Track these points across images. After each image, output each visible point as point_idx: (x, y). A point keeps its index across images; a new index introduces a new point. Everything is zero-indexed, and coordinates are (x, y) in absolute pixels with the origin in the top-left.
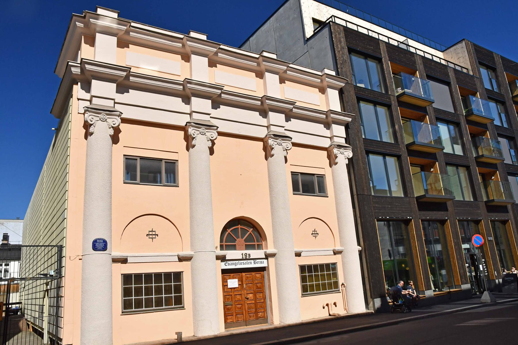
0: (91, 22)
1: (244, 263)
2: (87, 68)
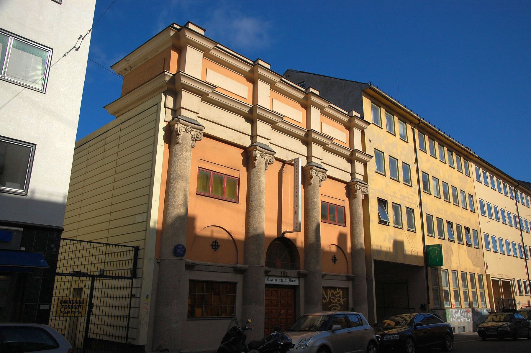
0: (186, 37)
1: (282, 280)
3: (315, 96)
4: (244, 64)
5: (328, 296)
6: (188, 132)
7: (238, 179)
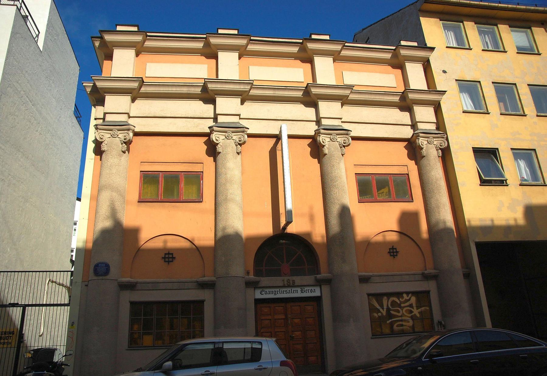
1: (288, 291)
2: (97, 86)
3: (316, 41)
4: (350, 50)
5: (385, 307)
6: (431, 143)
7: (407, 175)
